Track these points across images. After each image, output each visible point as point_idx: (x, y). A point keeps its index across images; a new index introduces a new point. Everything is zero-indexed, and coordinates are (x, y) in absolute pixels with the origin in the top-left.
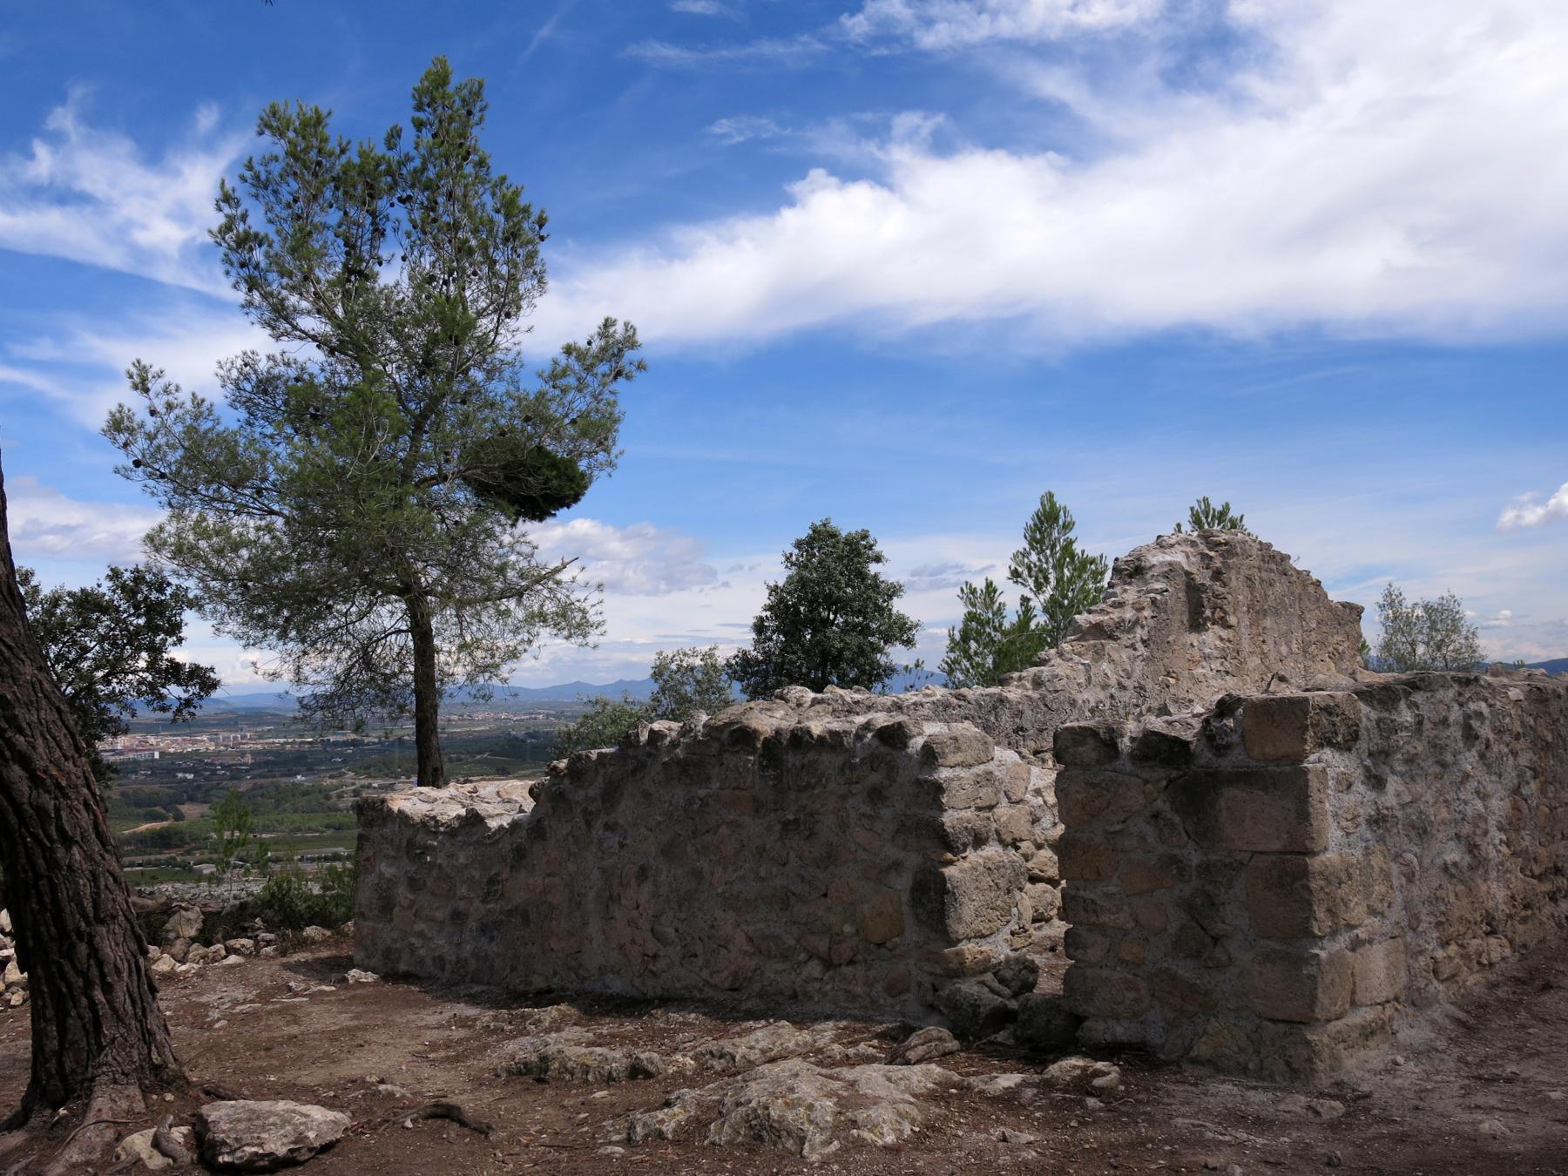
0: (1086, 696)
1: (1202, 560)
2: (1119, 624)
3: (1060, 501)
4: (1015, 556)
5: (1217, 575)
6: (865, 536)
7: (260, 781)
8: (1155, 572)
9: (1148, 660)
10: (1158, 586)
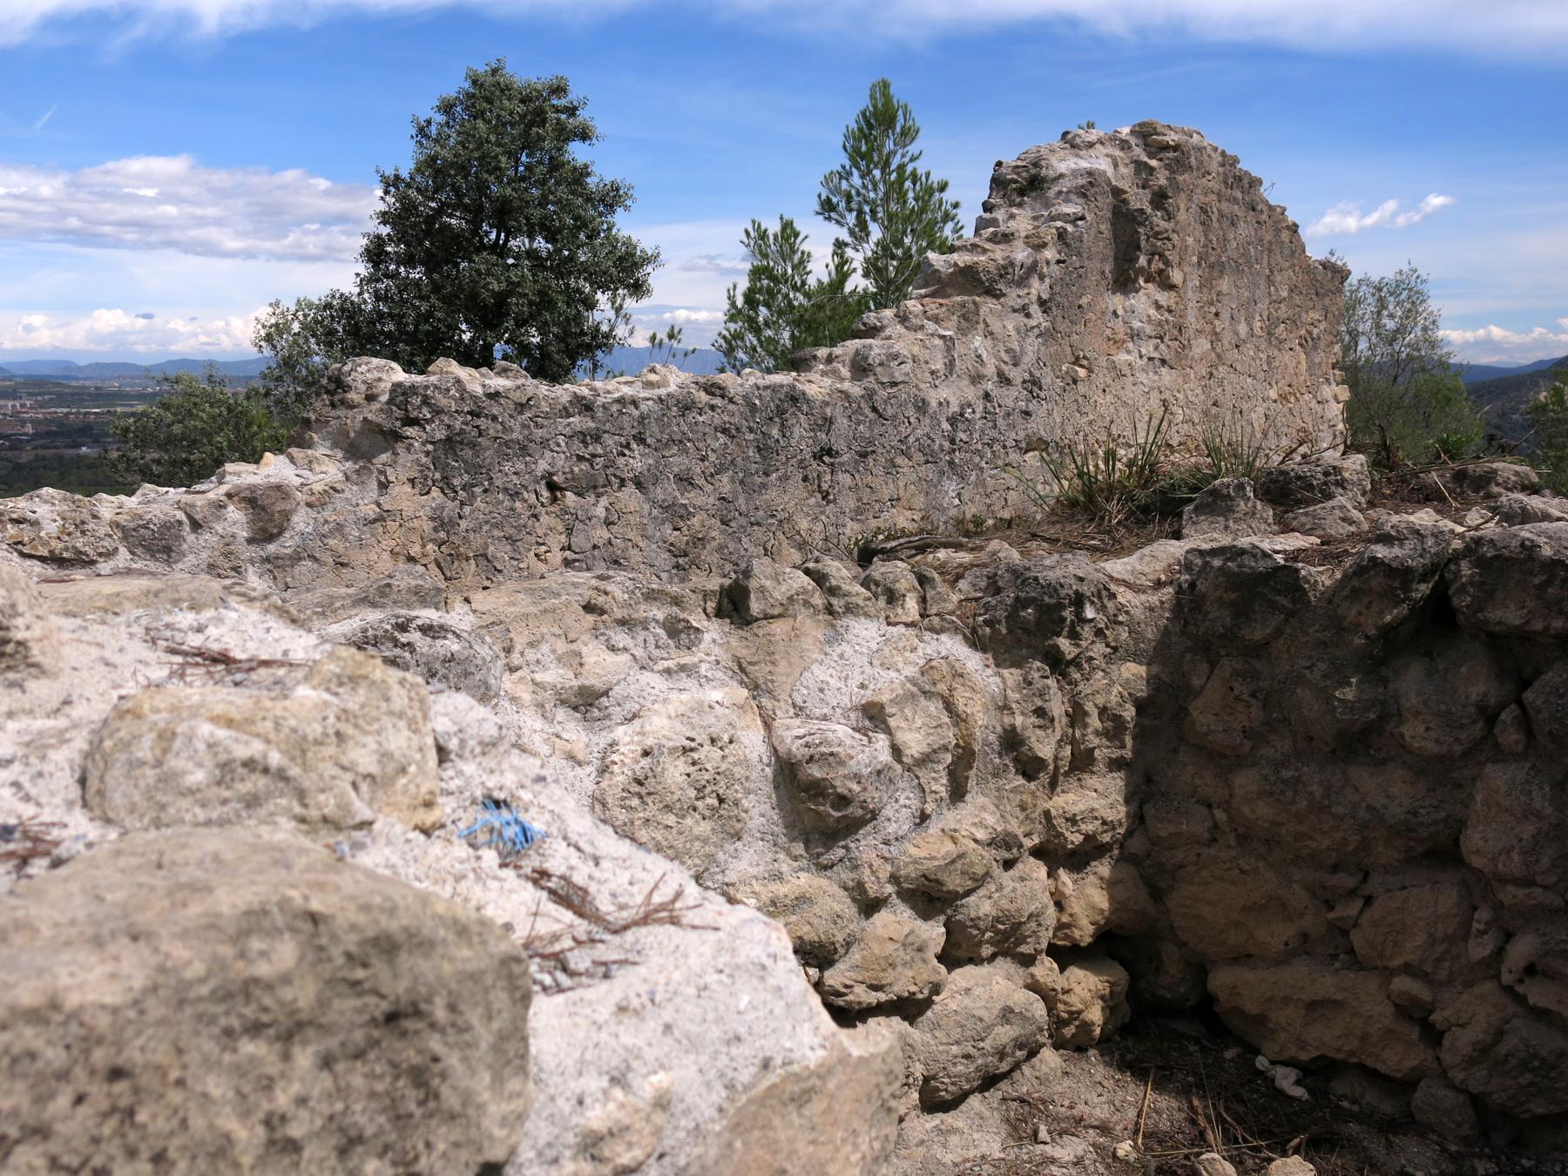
0: (944, 393)
1: (1137, 172)
2: (1005, 270)
3: (898, 93)
4: (827, 180)
5: (1160, 199)
6: (559, 90)
7: (41, 452)
8: (1064, 185)
9: (1047, 335)
10: (1069, 209)
